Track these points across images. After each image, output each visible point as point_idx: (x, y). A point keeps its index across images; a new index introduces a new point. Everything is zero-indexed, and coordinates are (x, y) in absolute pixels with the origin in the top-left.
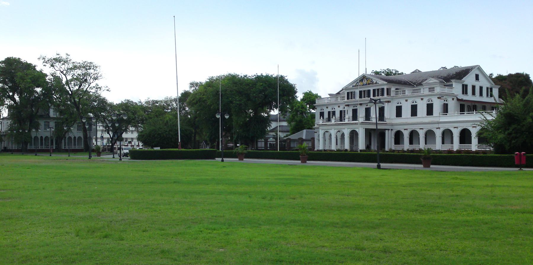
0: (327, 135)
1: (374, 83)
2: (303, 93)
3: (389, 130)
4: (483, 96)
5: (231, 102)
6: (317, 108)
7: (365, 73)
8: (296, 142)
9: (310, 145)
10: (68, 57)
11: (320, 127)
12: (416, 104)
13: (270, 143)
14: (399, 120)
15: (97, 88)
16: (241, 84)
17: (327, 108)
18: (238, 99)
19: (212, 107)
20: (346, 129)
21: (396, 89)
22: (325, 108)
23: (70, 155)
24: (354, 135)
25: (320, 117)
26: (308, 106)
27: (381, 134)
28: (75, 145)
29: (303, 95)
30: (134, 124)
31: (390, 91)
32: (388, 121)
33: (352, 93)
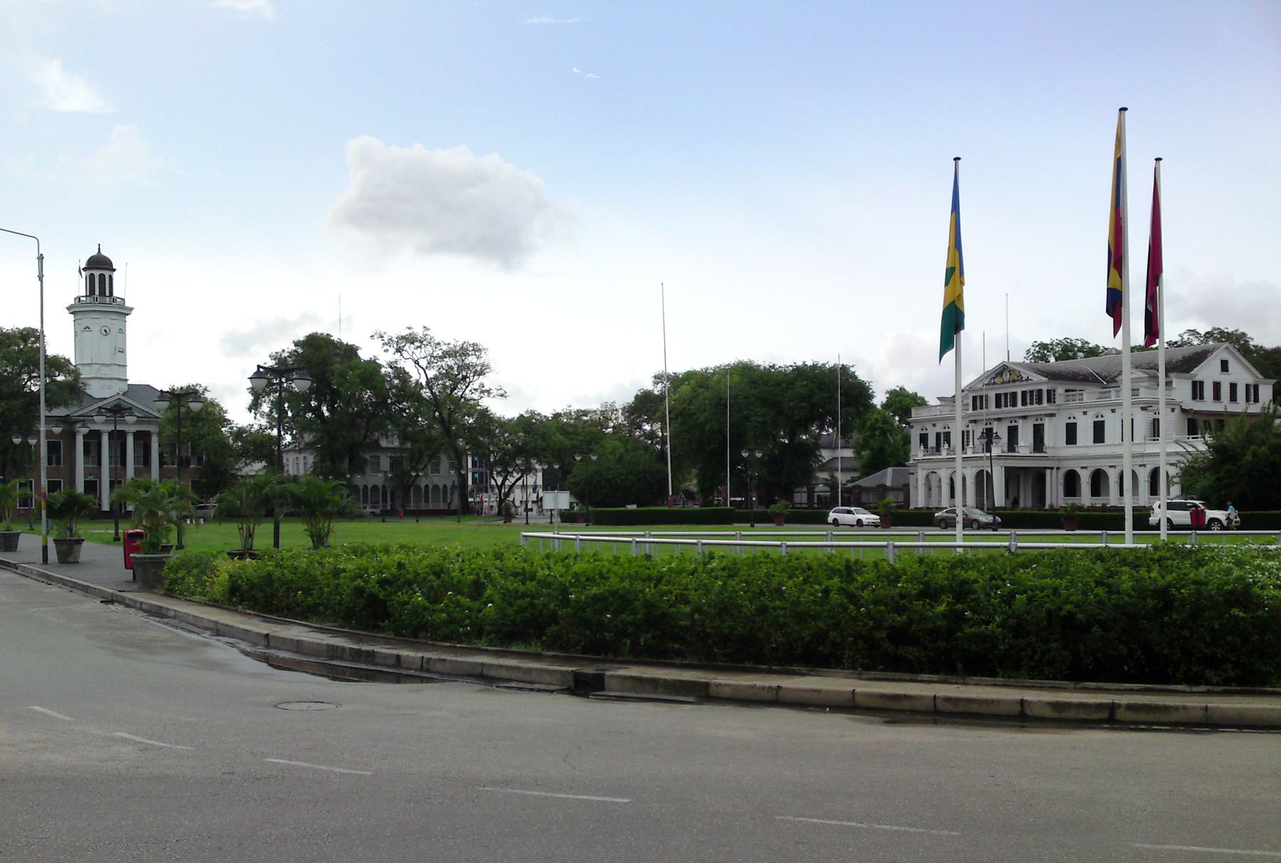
0: (934, 478)
1: (1024, 379)
2: (887, 392)
3: (1052, 468)
4: (1238, 401)
5: (747, 418)
6: (915, 427)
7: (1006, 360)
8: (872, 494)
9: (901, 498)
10: (426, 332)
11: (919, 465)
12: (1102, 419)
13: (818, 496)
14: (1071, 451)
15: (483, 392)
16: (765, 383)
17: (934, 425)
18: (759, 414)
19: (707, 428)
20: (944, 470)
21: (1067, 391)
22: (929, 426)
23: (460, 520)
24: (983, 480)
25: (920, 443)
26: (897, 418)
27: (1039, 476)
28: (427, 501)
29: (888, 395)
30: (547, 460)
31: (1054, 395)
32: (1050, 453)
33: (981, 397)
